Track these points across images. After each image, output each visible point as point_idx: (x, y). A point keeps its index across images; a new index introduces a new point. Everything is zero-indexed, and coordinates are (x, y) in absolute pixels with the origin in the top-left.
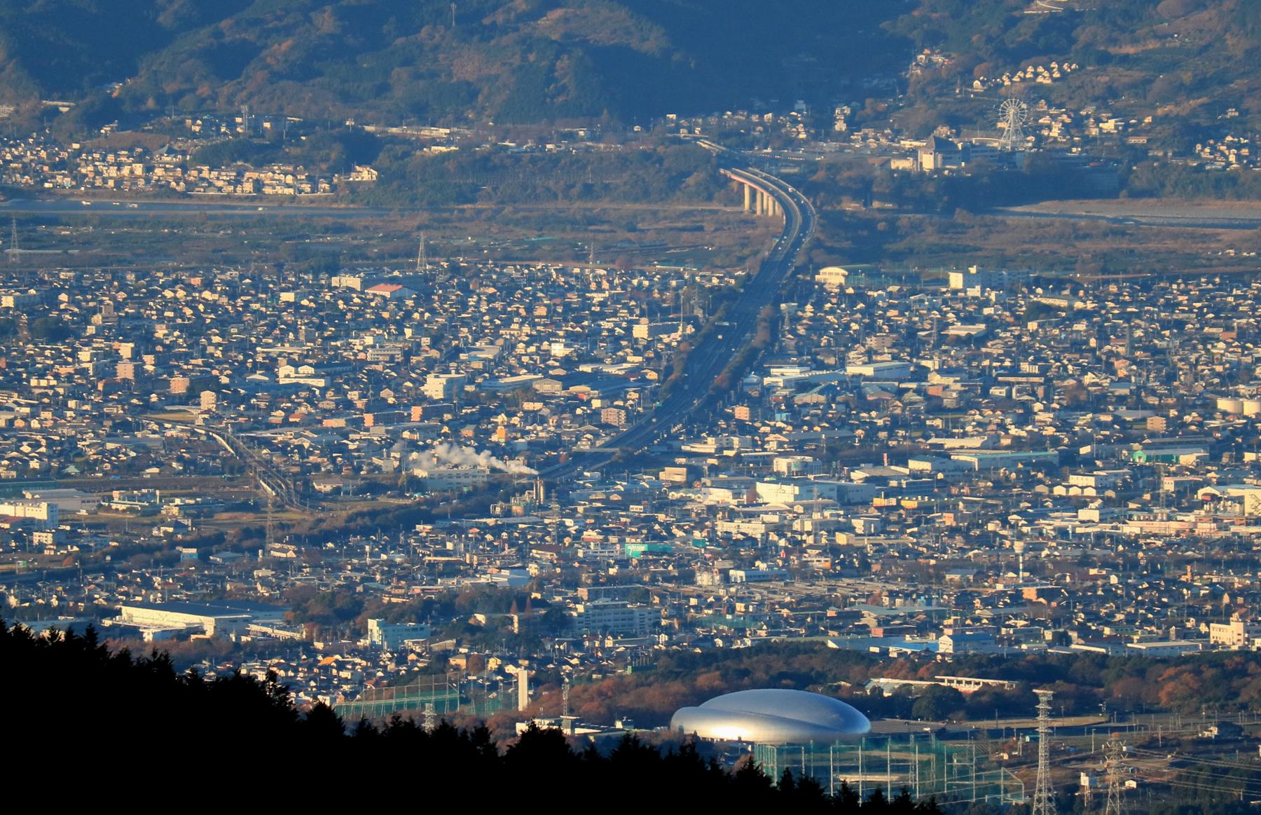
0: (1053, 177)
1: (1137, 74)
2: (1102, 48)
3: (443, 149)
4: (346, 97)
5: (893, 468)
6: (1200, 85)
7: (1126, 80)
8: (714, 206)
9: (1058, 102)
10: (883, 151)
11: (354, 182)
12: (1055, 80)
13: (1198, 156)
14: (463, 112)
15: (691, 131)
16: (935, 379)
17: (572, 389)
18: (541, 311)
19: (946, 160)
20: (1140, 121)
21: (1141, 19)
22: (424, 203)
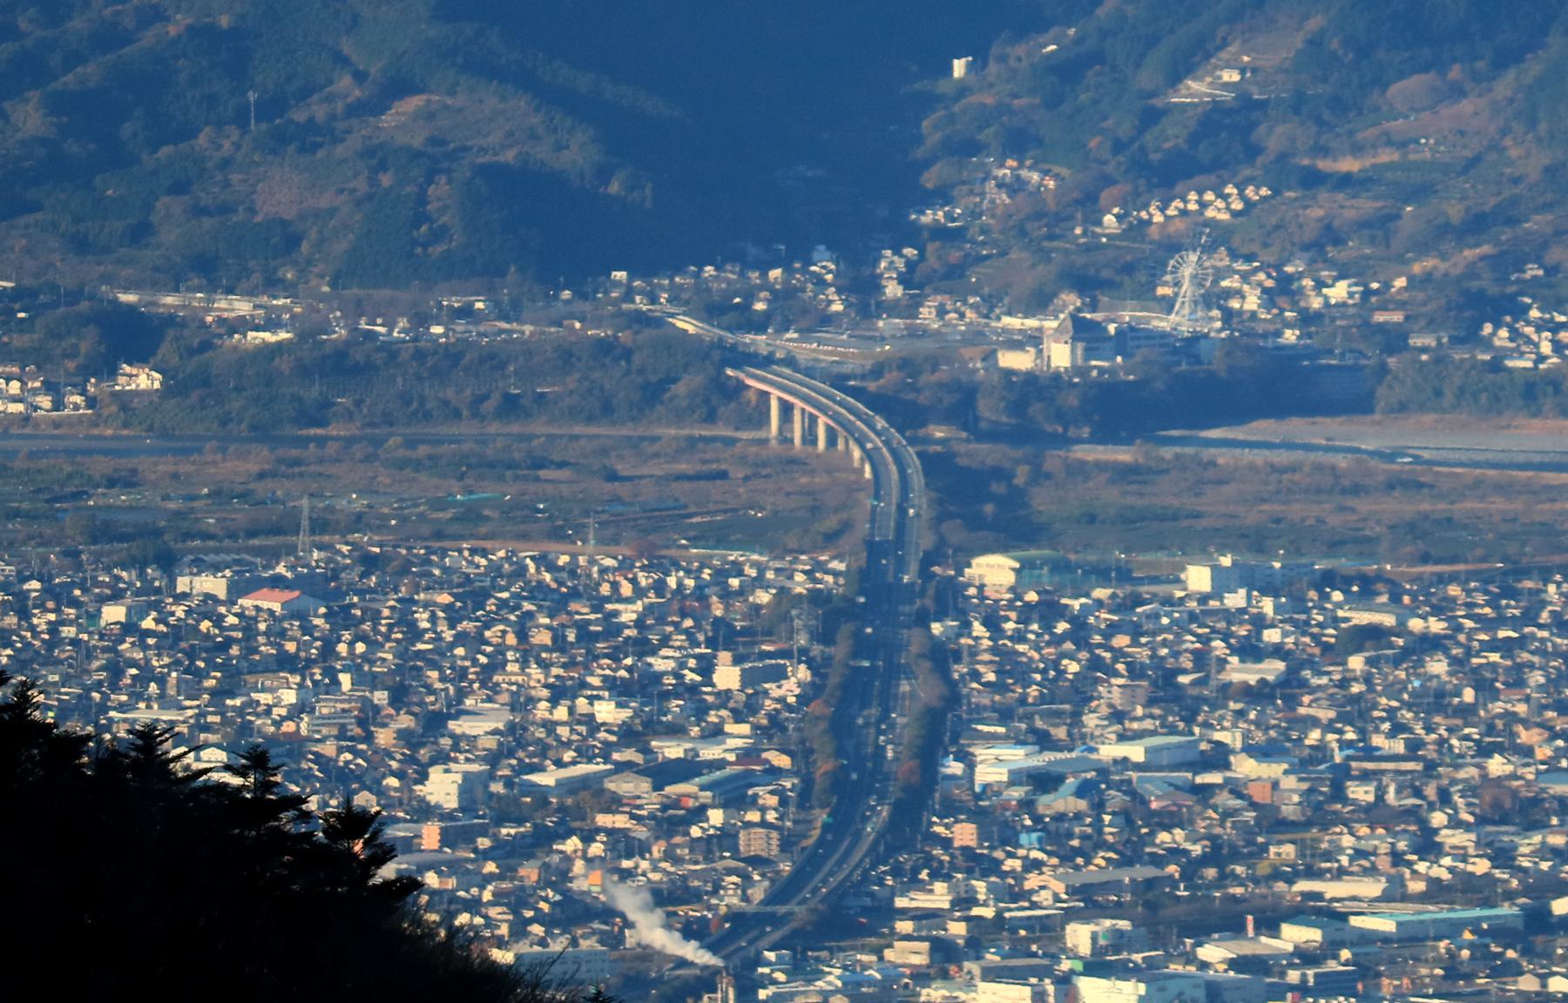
0: (1264, 382)
1: (1366, 205)
2: (1306, 162)
3: (268, 336)
4: (81, 245)
5: (1263, 939)
6: (1476, 225)
7: (1349, 214)
8: (722, 431)
9: (1245, 250)
10: (976, 336)
11: (123, 392)
12: (1235, 214)
13: (1487, 344)
14: (275, 270)
15: (653, 300)
16: (1245, 767)
17: (669, 790)
18: (542, 637)
19: (1090, 353)
20: (1387, 285)
21: (1360, 113)
22: (243, 426)
